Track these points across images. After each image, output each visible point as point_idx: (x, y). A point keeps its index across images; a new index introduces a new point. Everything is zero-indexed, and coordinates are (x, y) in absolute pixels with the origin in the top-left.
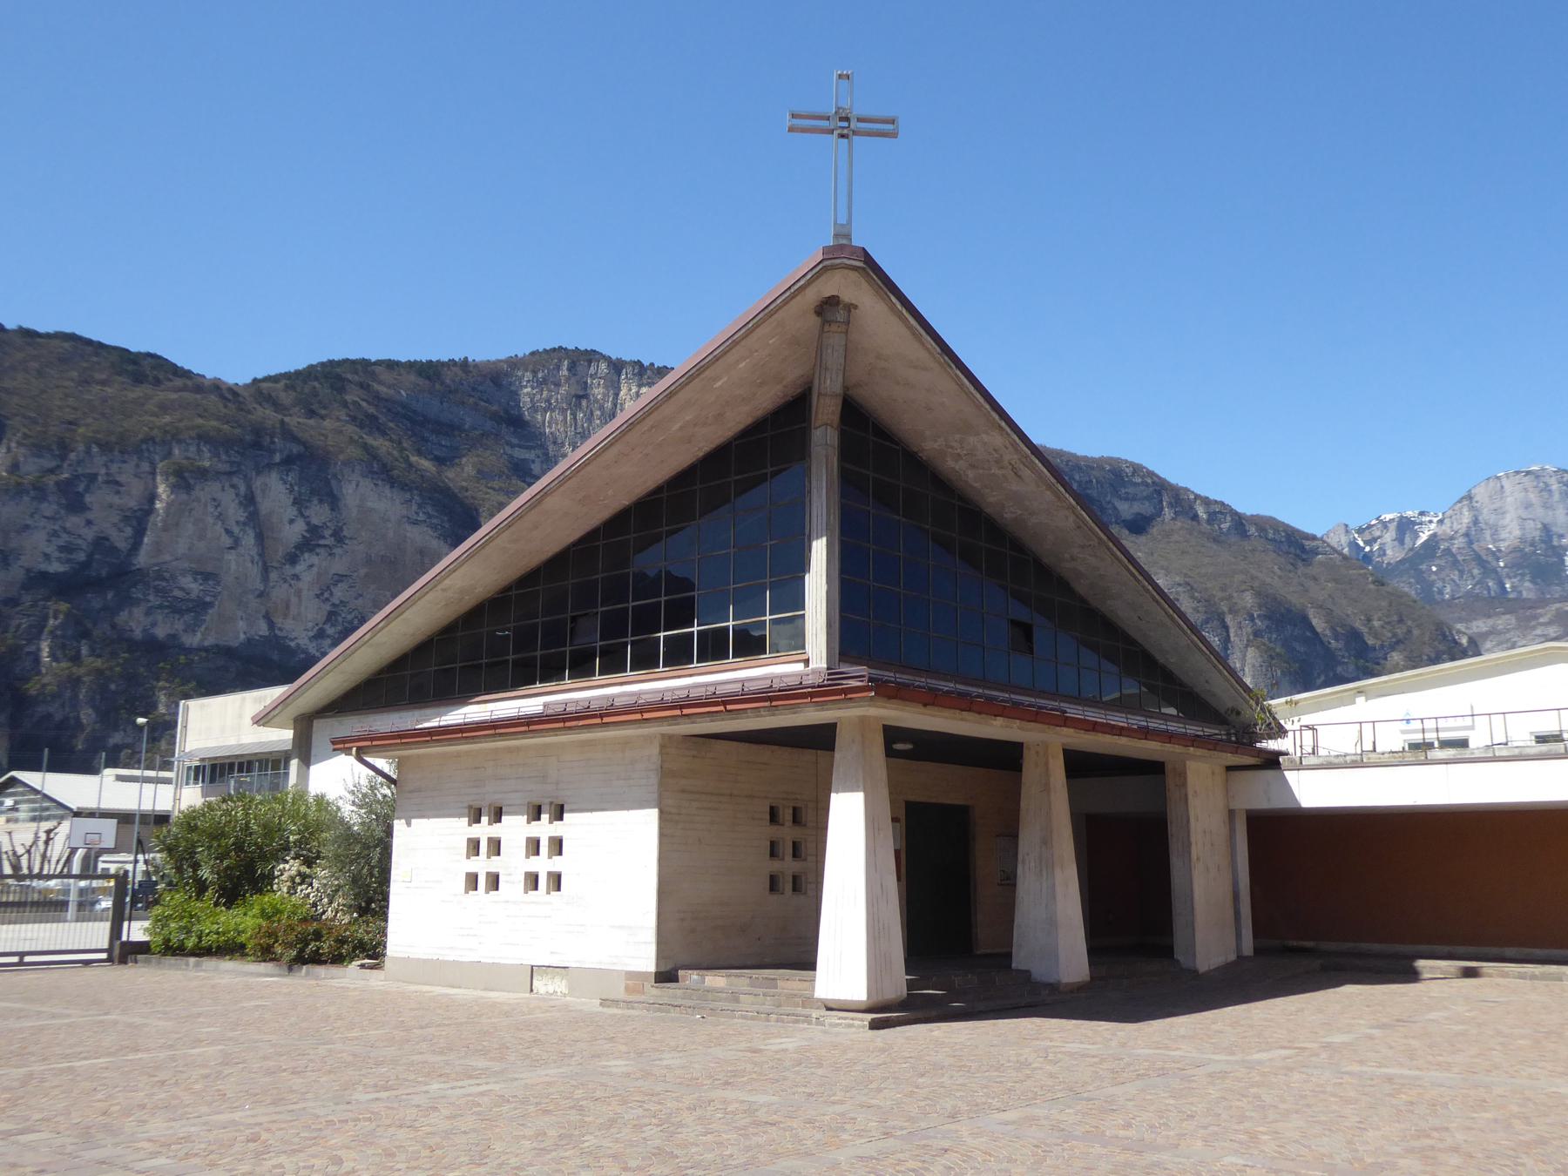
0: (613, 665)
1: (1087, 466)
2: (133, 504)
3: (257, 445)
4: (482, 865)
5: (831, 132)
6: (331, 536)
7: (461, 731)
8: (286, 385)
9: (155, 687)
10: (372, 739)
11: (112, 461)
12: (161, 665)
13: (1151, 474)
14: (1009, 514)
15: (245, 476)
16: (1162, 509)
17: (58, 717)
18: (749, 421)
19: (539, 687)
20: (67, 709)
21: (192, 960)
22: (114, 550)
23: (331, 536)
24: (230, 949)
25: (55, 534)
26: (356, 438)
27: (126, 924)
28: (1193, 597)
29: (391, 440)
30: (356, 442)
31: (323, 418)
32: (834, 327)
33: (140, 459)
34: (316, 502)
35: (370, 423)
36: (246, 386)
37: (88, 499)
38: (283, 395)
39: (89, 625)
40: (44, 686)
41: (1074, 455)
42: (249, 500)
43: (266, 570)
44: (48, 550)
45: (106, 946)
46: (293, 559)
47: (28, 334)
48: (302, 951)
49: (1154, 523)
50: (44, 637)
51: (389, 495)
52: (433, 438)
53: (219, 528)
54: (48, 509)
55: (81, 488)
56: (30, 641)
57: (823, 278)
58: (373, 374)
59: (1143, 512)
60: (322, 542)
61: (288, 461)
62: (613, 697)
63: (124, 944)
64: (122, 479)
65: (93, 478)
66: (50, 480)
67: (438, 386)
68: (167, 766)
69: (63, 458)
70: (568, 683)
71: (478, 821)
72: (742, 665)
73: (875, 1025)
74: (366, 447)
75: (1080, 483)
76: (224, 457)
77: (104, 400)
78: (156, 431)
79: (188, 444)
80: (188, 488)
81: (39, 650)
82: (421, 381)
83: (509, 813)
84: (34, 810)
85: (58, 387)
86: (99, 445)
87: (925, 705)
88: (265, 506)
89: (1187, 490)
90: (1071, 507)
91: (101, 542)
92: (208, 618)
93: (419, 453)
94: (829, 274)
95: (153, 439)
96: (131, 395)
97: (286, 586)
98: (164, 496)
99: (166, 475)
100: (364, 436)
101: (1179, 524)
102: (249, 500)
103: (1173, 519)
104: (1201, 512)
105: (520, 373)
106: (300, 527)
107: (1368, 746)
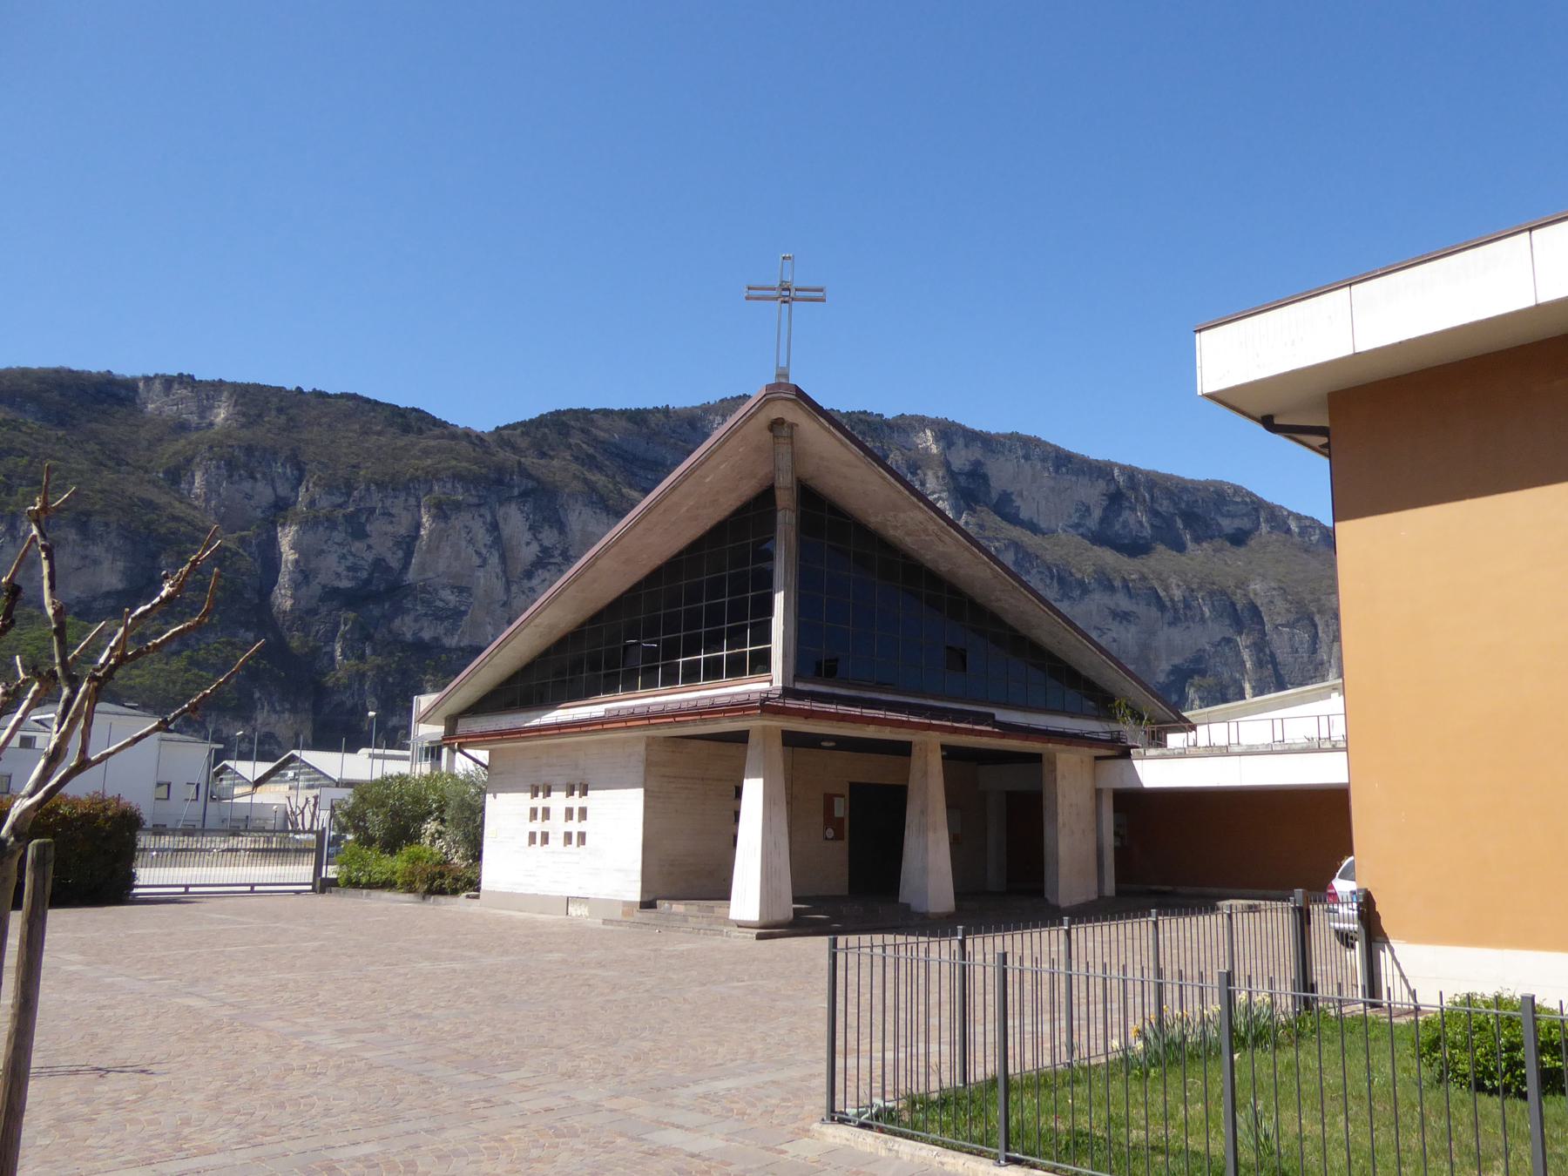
0: (650, 683)
1: (1194, 488)
2: (403, 531)
3: (499, 482)
4: (538, 826)
5: (776, 299)
6: (560, 555)
7: (539, 730)
8: (522, 433)
9: (423, 680)
10: (467, 737)
11: (386, 497)
12: (427, 662)
13: (1250, 494)
14: (943, 567)
15: (490, 508)
16: (1259, 524)
17: (349, 704)
18: (739, 504)
19: (602, 697)
20: (356, 697)
21: (365, 891)
22: (389, 569)
23: (560, 555)
24: (388, 885)
25: (344, 557)
26: (579, 474)
27: (324, 867)
28: (1286, 600)
29: (607, 476)
30: (578, 477)
31: (552, 458)
32: (781, 440)
33: (408, 494)
34: (547, 527)
35: (590, 462)
36: (491, 433)
37: (368, 528)
38: (519, 441)
39: (372, 631)
40: (338, 679)
41: (1182, 479)
42: (494, 527)
43: (508, 584)
44: (340, 570)
45: (311, 881)
46: (529, 575)
47: (321, 395)
48: (431, 885)
49: (1253, 536)
50: (337, 640)
51: (606, 521)
52: (642, 473)
53: (471, 550)
54: (338, 536)
55: (363, 519)
56: (326, 644)
57: (768, 407)
58: (592, 421)
59: (1243, 527)
60: (552, 560)
61: (525, 494)
62: (648, 706)
63: (322, 880)
64: (394, 511)
65: (372, 511)
66: (339, 513)
67: (645, 430)
68: (405, 747)
69: (349, 495)
70: (621, 695)
71: (537, 796)
72: (730, 683)
73: (760, 937)
74: (586, 481)
75: (1187, 503)
76: (473, 492)
77: (380, 448)
78: (419, 472)
79: (445, 482)
80: (446, 518)
81: (334, 651)
82: (630, 426)
83: (555, 791)
84: (309, 780)
85: (344, 438)
86: (377, 484)
87: (806, 718)
88: (506, 531)
89: (1281, 507)
90: (985, 563)
91: (379, 563)
92: (463, 623)
93: (631, 486)
94: (771, 405)
95: (417, 478)
96: (400, 443)
97: (524, 597)
98: (427, 525)
99: (429, 508)
100: (586, 473)
101: (1274, 537)
102: (494, 527)
103: (1269, 532)
104: (1294, 527)
105: (711, 418)
106: (535, 548)
107: (1234, 740)
